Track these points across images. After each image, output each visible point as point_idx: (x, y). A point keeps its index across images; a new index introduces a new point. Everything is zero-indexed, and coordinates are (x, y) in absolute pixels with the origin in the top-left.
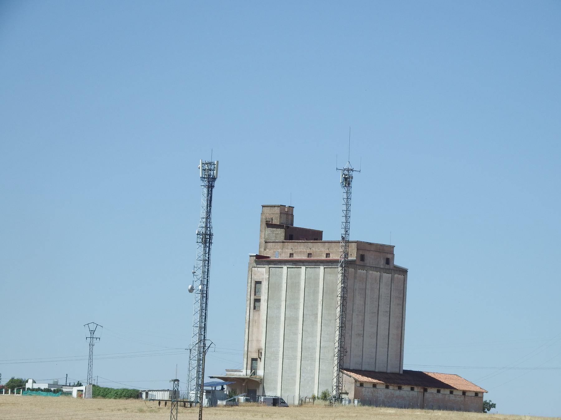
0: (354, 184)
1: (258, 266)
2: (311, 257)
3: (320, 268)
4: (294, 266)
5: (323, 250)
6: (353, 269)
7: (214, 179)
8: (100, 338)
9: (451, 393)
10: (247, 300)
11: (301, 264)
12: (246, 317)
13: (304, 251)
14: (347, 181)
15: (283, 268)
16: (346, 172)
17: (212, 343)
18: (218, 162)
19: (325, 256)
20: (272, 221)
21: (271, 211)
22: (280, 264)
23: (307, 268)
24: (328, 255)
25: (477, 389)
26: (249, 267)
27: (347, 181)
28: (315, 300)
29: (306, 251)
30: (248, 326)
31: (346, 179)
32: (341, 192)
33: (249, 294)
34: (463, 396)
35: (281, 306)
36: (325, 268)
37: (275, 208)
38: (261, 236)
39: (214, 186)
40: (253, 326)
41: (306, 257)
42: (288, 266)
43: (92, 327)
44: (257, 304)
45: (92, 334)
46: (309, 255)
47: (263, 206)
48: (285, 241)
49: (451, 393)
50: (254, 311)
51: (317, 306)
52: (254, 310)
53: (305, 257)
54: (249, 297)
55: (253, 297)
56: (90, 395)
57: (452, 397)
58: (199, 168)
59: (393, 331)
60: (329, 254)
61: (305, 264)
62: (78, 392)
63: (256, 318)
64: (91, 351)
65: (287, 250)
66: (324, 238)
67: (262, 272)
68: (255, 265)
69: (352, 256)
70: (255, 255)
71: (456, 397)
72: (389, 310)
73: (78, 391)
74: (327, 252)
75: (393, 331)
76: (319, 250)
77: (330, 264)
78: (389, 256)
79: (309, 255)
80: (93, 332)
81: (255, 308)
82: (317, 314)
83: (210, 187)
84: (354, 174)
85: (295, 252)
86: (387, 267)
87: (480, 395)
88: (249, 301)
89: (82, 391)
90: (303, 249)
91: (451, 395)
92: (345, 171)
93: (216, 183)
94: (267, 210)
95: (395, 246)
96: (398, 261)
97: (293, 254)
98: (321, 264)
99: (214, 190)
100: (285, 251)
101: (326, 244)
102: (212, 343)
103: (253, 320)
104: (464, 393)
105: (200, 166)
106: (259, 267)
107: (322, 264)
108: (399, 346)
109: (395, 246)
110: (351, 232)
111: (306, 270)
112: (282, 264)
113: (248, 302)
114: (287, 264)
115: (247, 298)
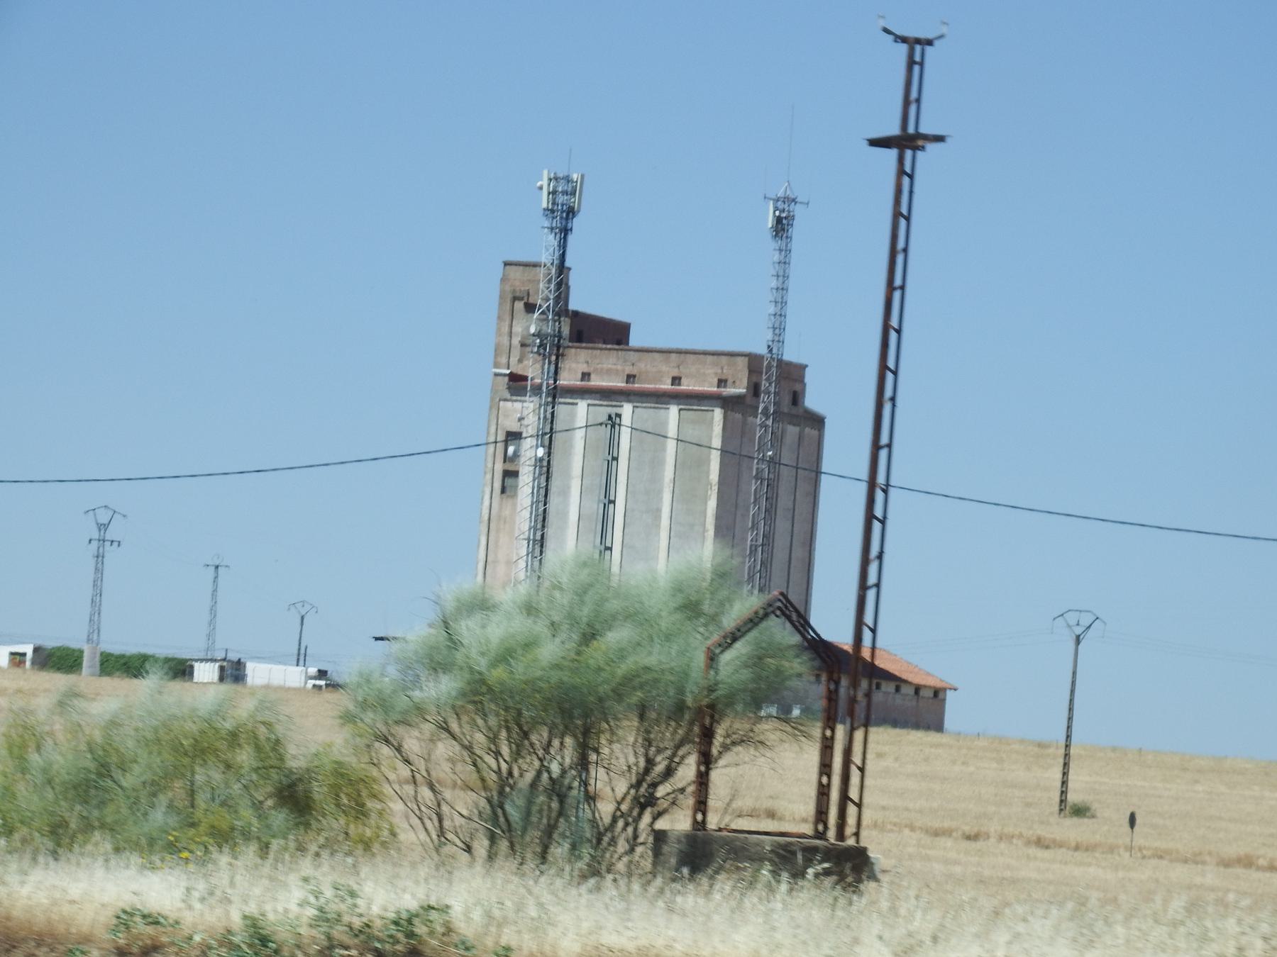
0: (798, 231)
1: (514, 398)
2: (633, 383)
3: (713, 411)
4: (605, 403)
5: (664, 368)
6: (740, 415)
7: (571, 212)
8: (119, 542)
9: (898, 689)
10: (485, 473)
11: (623, 398)
12: (481, 510)
13: (617, 370)
14: (781, 226)
15: (577, 404)
16: (780, 205)
17: (1097, 618)
18: (583, 176)
19: (669, 381)
20: (528, 298)
21: (526, 275)
22: (569, 395)
23: (637, 407)
24: (676, 380)
25: (939, 685)
26: (492, 399)
27: (781, 226)
28: (656, 479)
29: (623, 371)
30: (487, 530)
31: (779, 220)
32: (769, 247)
33: (490, 459)
34: (916, 697)
35: (569, 487)
36: (680, 410)
37: (534, 268)
38: (499, 330)
39: (571, 230)
40: (498, 531)
41: (622, 383)
42: (590, 402)
43: (103, 517)
44: (509, 481)
45: (102, 532)
46: (630, 378)
47: (506, 264)
48: (570, 344)
49: (898, 689)
50: (502, 499)
51: (660, 492)
52: (503, 495)
53: (620, 384)
54: (490, 465)
55: (499, 467)
56: (95, 667)
57: (898, 700)
58: (541, 188)
59: (798, 553)
60: (680, 378)
61: (632, 398)
62: (13, 657)
63: (507, 512)
64: (99, 570)
65: (574, 365)
66: (635, 340)
67: (526, 413)
68: (508, 396)
69: (737, 385)
70: (508, 372)
71: (904, 699)
72: (792, 506)
73: (12, 654)
74: (675, 373)
75: (798, 553)
76: (654, 370)
77: (696, 401)
78: (798, 387)
79: (630, 378)
80: (103, 527)
81: (503, 490)
82: (659, 510)
83: (565, 232)
84: (798, 211)
85: (596, 370)
86: (794, 411)
87: (941, 695)
88: (491, 475)
89: (24, 655)
90: (615, 364)
91: (898, 696)
92: (779, 203)
93: (577, 223)
94: (515, 273)
95: (806, 366)
96: (812, 402)
97: (589, 374)
98: (672, 401)
99: (571, 238)
100: (570, 366)
101: (673, 356)
102: (1097, 618)
103: (499, 517)
104: (917, 689)
105: (545, 182)
106: (516, 401)
107: (675, 401)
108: (805, 586)
109: (806, 366)
110: (789, 336)
111: (633, 412)
112: (575, 396)
113: (489, 476)
114: (587, 396)
115: (486, 466)
